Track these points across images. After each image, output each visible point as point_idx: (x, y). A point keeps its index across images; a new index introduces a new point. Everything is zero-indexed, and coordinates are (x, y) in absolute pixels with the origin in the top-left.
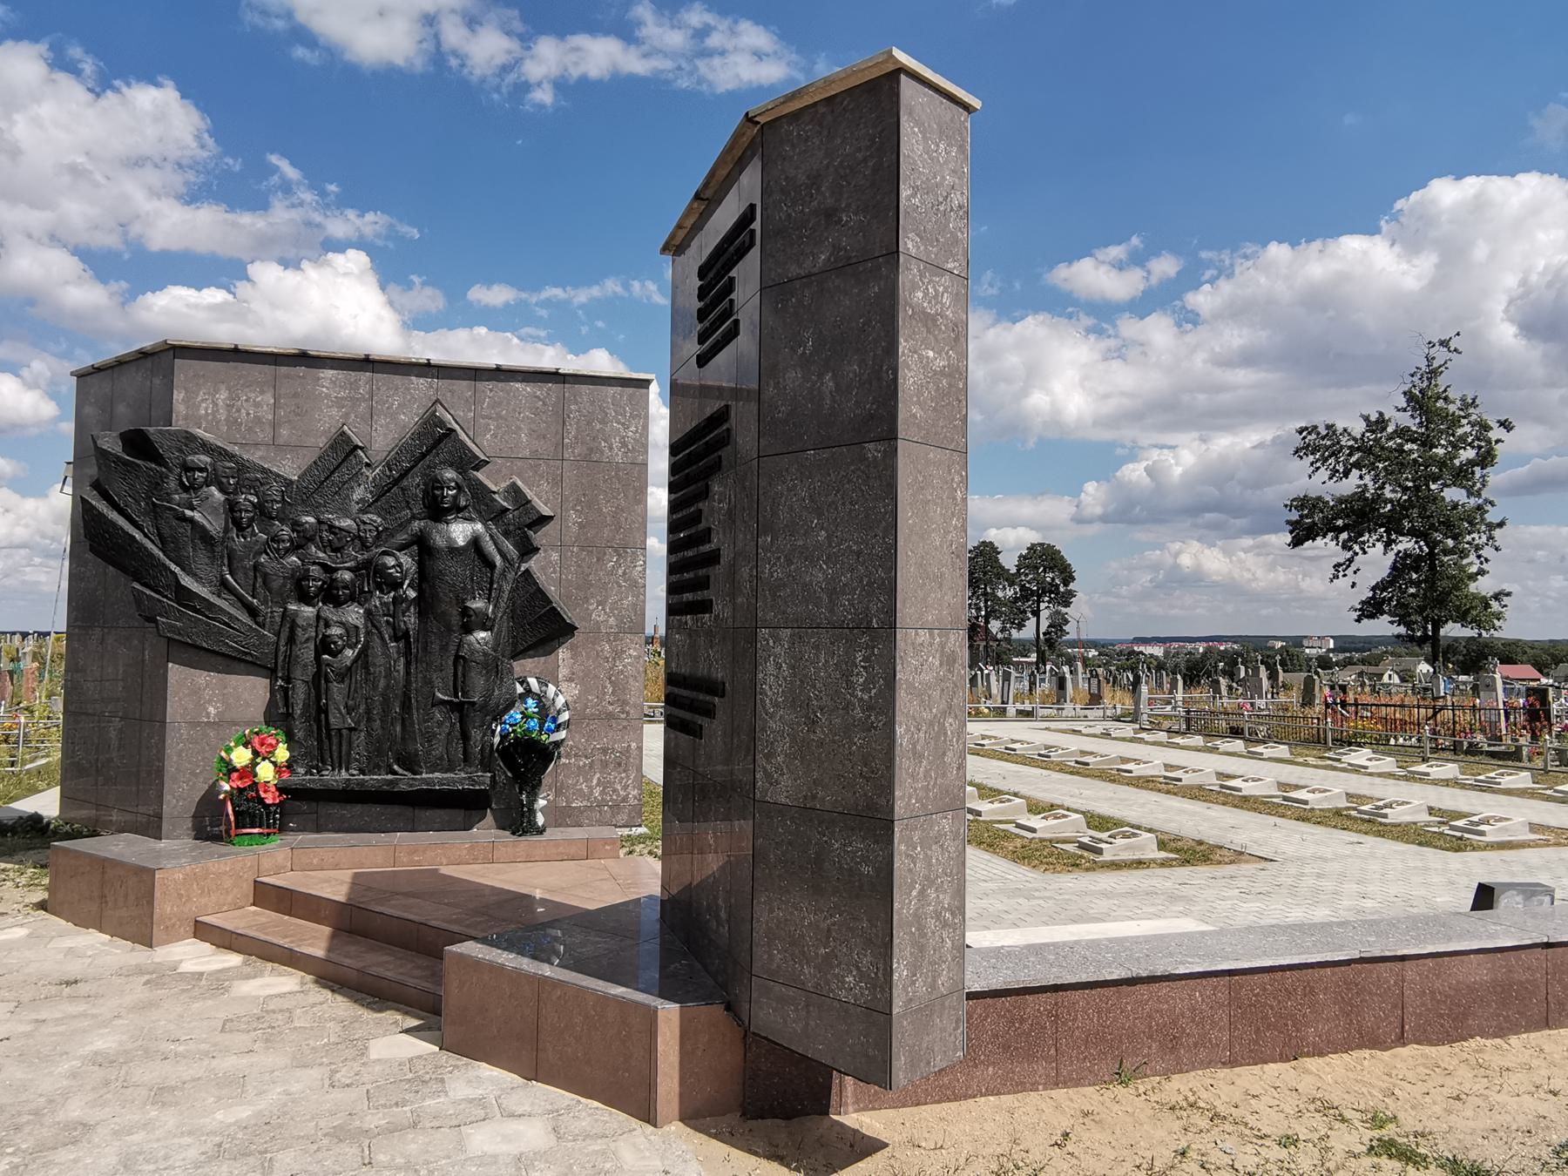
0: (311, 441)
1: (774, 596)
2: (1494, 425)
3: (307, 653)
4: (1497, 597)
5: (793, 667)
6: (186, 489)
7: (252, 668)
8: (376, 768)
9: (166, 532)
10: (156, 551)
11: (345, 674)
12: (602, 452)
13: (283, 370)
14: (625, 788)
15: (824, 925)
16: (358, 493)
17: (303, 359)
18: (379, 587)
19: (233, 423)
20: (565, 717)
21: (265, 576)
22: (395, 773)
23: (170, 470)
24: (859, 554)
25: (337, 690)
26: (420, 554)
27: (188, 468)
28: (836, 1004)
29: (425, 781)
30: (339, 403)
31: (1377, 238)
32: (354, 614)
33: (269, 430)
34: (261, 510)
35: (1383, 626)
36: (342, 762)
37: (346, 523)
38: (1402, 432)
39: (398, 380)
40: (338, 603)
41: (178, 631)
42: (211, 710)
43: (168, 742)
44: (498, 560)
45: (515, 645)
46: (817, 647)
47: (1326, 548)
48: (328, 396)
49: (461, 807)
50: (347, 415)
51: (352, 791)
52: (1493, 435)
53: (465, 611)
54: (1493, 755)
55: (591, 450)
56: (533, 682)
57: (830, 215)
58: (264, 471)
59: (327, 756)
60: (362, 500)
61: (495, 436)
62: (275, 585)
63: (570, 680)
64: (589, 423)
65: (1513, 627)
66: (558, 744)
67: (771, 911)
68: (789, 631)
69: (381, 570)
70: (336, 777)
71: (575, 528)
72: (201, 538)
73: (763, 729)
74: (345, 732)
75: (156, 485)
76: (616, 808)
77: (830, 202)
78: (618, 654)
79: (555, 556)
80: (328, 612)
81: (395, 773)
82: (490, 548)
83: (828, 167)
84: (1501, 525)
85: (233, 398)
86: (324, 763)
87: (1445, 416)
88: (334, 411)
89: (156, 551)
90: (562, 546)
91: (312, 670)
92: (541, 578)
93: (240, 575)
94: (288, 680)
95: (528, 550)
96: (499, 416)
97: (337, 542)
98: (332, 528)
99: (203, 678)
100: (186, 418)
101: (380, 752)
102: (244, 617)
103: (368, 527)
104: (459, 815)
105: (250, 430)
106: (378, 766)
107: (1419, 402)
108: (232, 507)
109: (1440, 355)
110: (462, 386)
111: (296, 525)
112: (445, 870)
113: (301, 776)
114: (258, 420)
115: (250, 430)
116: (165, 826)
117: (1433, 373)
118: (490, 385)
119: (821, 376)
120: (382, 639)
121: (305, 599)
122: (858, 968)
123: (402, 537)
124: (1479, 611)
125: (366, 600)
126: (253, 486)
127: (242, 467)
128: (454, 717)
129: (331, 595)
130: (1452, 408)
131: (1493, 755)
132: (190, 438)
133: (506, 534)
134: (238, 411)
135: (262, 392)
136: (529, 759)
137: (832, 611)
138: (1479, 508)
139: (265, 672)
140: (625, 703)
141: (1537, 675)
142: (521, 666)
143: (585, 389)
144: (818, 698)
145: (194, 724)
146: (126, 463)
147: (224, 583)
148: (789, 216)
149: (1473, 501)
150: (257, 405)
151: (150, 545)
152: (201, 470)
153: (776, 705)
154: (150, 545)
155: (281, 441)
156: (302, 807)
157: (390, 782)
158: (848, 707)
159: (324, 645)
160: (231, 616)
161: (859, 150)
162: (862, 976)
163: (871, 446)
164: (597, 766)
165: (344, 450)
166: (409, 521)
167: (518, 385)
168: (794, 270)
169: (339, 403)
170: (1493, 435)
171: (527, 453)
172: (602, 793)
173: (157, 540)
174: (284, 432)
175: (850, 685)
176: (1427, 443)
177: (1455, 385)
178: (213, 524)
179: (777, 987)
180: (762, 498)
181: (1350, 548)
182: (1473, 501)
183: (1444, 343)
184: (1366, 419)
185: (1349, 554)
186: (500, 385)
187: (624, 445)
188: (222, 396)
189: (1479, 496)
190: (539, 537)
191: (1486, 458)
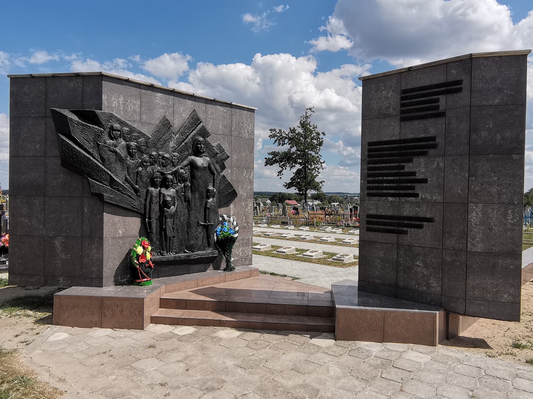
0: (153, 122)
1: (476, 195)
2: (321, 134)
3: (156, 208)
4: (321, 183)
5: (483, 214)
6: (112, 138)
7: (135, 214)
8: (180, 251)
9: (105, 157)
10: (101, 165)
11: (173, 216)
12: (242, 134)
13: (143, 91)
14: (248, 252)
15: (496, 283)
16: (172, 144)
17: (151, 87)
18: (179, 181)
19: (126, 111)
20: (237, 229)
21: (141, 176)
22: (187, 253)
23: (105, 130)
24: (510, 184)
25: (169, 221)
26: (191, 169)
27: (112, 129)
28: (500, 303)
29: (198, 255)
30: (163, 107)
31: (249, 67)
32: (171, 191)
33: (138, 115)
34: (138, 148)
35: (293, 190)
36: (169, 251)
37: (167, 155)
38: (299, 134)
39: (182, 100)
40: (167, 187)
41: (111, 199)
42: (120, 232)
43: (104, 246)
44: (215, 172)
45: (220, 203)
46: (493, 209)
47: (276, 167)
48: (159, 104)
49: (203, 263)
50: (165, 112)
51: (176, 260)
52: (320, 137)
53: (208, 191)
54: (354, 227)
55: (239, 133)
56: (225, 216)
57: (500, 90)
58: (140, 133)
59: (164, 247)
60: (173, 147)
61: (212, 125)
62: (145, 180)
63: (234, 215)
64: (239, 123)
65: (325, 189)
66: (237, 238)
67: (474, 281)
68: (482, 204)
69: (181, 175)
70: (171, 256)
71: (235, 161)
72: (119, 160)
73: (471, 231)
74: (172, 238)
75: (98, 136)
76: (246, 259)
77: (500, 86)
78: (247, 206)
79: (230, 171)
80: (164, 191)
81: (187, 253)
82: (212, 167)
83: (499, 76)
84: (324, 163)
85: (125, 101)
86: (163, 250)
87: (308, 129)
88: (161, 110)
89: (101, 165)
90: (231, 168)
91: (158, 214)
92: (229, 178)
93: (132, 176)
94: (150, 218)
95: (223, 167)
96: (213, 118)
97: (165, 162)
98: (163, 157)
99: (117, 219)
100: (108, 107)
101: (181, 245)
102: (133, 192)
103: (176, 158)
104: (202, 266)
105: (132, 115)
106: (181, 250)
107: (303, 125)
108: (128, 147)
109: (309, 113)
110: (202, 105)
111: (151, 156)
112: (217, 286)
113: (158, 257)
114: (134, 111)
115: (132, 115)
116: (104, 281)
117: (307, 117)
118: (211, 106)
119: (495, 134)
120: (182, 201)
121: (154, 185)
122: (509, 293)
123: (185, 162)
124: (316, 187)
125: (176, 187)
126: (136, 139)
127: (132, 130)
128: (205, 230)
129: (165, 183)
130: (311, 128)
131: (354, 227)
132: (112, 116)
133: (217, 162)
134: (127, 106)
135: (136, 100)
136: (226, 244)
137: (499, 199)
138: (318, 157)
139: (140, 216)
140: (248, 223)
141: (297, 203)
142: (221, 211)
143: (238, 111)
144: (493, 223)
145: (114, 238)
146: (82, 125)
147: (126, 180)
148: (483, 87)
149: (316, 155)
150: (134, 105)
151: (99, 164)
152: (119, 131)
153: (477, 225)
154: (99, 164)
155: (143, 121)
156: (162, 268)
157: (188, 256)
158: (505, 225)
159: (165, 204)
160: (131, 193)
161: (512, 74)
162: (510, 295)
163: (515, 156)
164: (241, 245)
165: (166, 125)
166: (187, 156)
167: (219, 107)
168: (485, 103)
169: (163, 107)
170: (320, 137)
171: (221, 133)
172: (242, 254)
173: (99, 160)
174: (144, 117)
175: (506, 219)
176: (305, 138)
177: (312, 122)
178: (123, 153)
179: (477, 302)
180: (471, 167)
181: (282, 168)
182: (316, 155)
183: (310, 109)
184: (290, 129)
185: (281, 169)
186: (214, 106)
187: (248, 132)
188: (121, 99)
189: (318, 153)
190: (227, 163)
191: (320, 144)
